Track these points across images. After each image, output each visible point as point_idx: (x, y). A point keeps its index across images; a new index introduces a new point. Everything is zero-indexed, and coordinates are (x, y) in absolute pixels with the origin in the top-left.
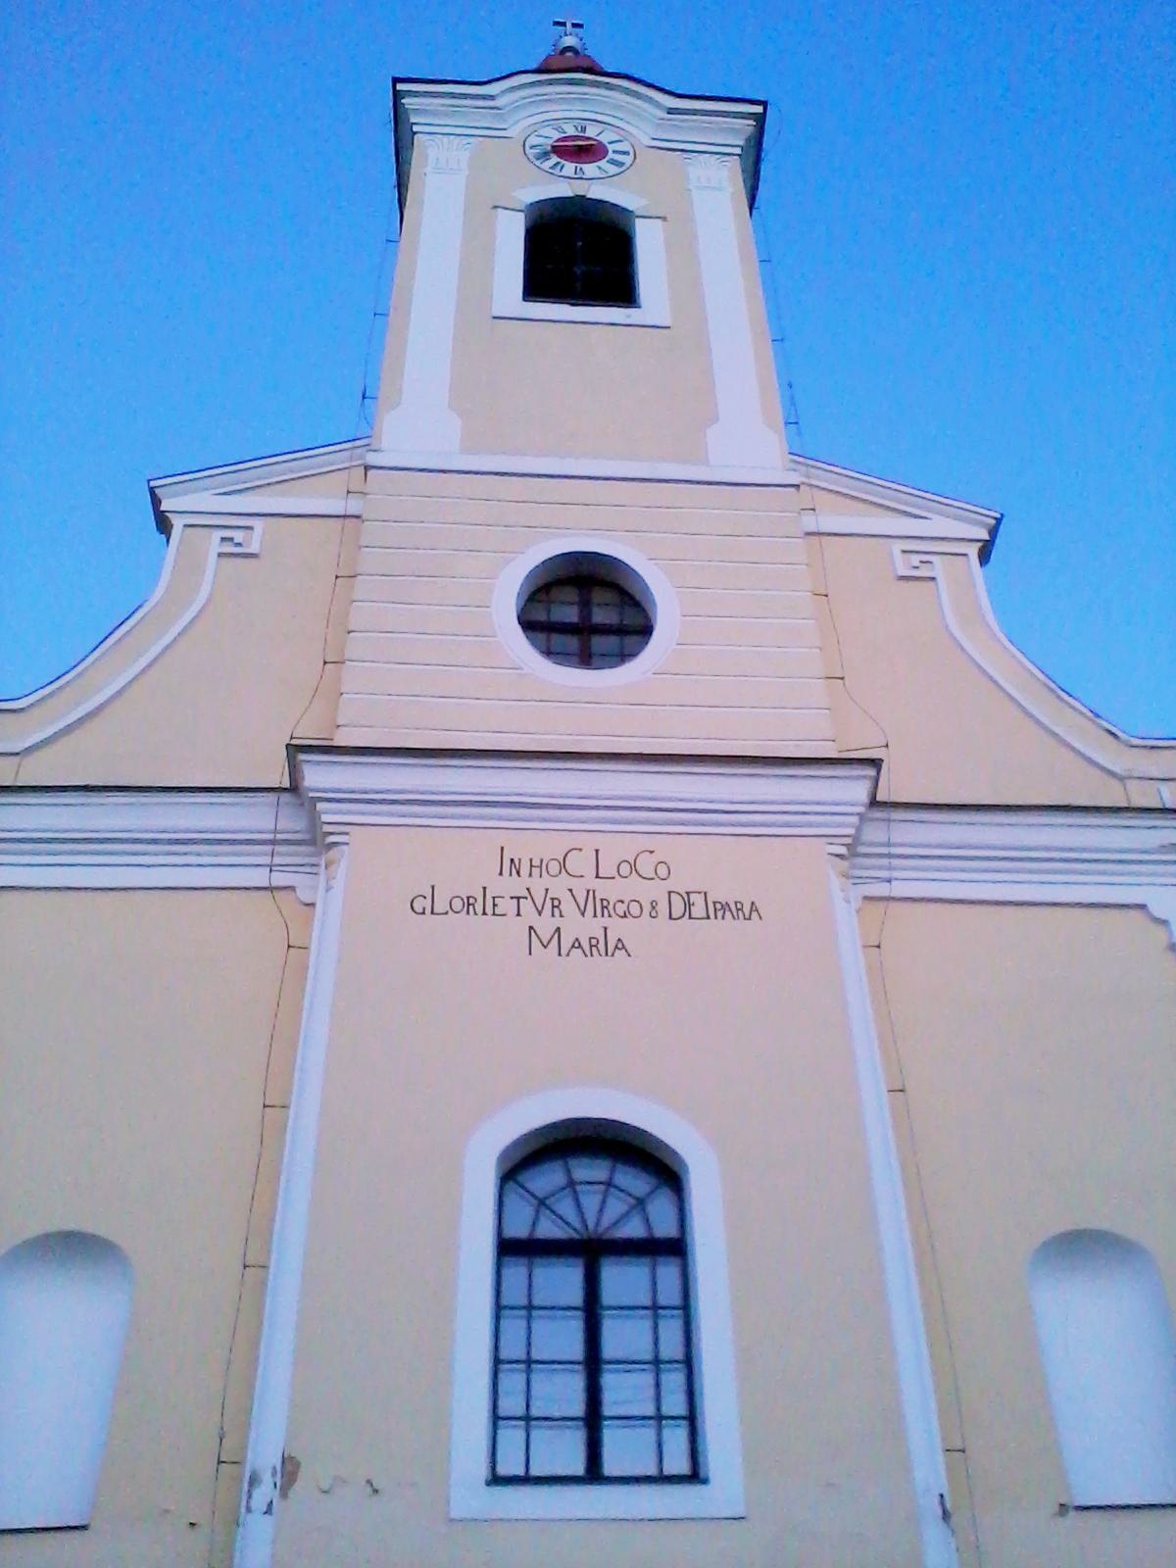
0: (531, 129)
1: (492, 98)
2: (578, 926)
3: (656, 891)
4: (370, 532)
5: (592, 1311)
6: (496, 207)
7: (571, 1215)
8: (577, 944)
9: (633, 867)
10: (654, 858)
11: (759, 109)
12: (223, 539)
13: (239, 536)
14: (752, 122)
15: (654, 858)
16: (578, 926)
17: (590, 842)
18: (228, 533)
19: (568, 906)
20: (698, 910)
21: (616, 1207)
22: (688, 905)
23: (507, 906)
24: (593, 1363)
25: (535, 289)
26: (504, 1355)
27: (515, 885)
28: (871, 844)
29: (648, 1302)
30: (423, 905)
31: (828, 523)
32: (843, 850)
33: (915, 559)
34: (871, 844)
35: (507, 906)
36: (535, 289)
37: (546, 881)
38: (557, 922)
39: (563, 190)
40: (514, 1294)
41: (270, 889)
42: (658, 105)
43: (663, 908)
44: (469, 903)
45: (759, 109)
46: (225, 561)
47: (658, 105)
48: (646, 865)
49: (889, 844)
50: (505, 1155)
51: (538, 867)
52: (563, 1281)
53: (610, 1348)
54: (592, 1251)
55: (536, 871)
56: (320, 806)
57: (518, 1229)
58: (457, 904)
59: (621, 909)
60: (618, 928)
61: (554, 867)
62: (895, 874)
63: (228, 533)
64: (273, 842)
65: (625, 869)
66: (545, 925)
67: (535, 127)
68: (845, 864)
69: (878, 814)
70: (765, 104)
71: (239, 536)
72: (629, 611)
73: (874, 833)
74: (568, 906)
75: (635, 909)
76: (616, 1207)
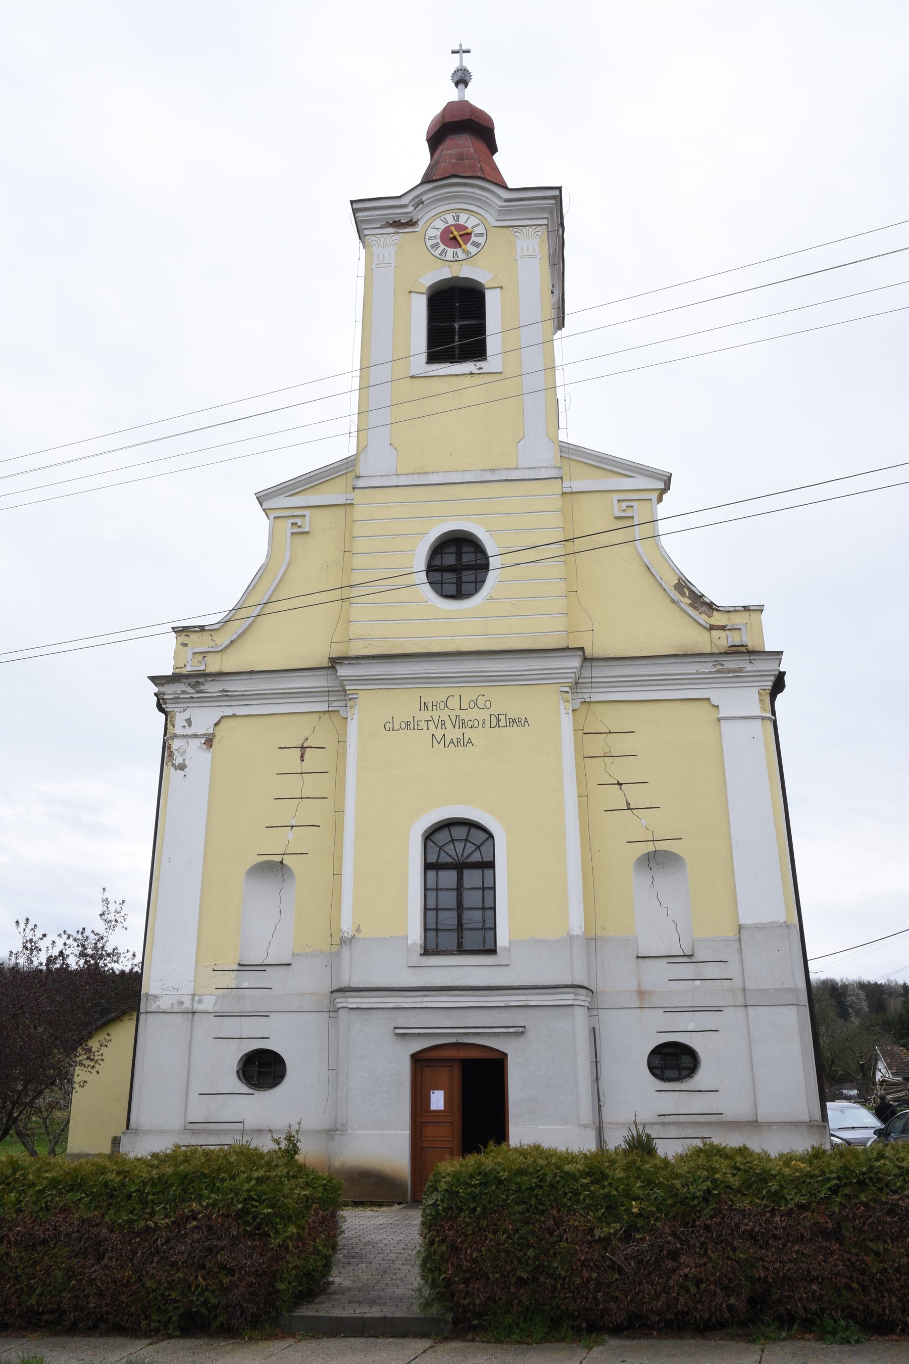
0: (428, 224)
1: (405, 206)
2: (453, 733)
3: (484, 715)
4: (359, 513)
5: (459, 888)
6: (410, 292)
7: (453, 853)
8: (452, 742)
9: (476, 704)
10: (485, 698)
11: (557, 193)
12: (292, 524)
13: (299, 521)
14: (553, 201)
15: (485, 698)
16: (453, 733)
17: (457, 693)
18: (294, 521)
19: (448, 724)
20: (502, 723)
21: (470, 848)
22: (498, 720)
23: (423, 725)
24: (460, 907)
25: (433, 358)
26: (428, 887)
27: (426, 715)
28: (585, 678)
29: (481, 892)
30: (388, 726)
31: (577, 486)
32: (567, 689)
33: (624, 505)
34: (585, 678)
35: (423, 725)
36: (433, 358)
37: (439, 712)
38: (444, 731)
39: (446, 273)
40: (431, 884)
41: (329, 711)
42: (499, 197)
43: (487, 723)
44: (408, 724)
45: (557, 193)
46: (296, 538)
47: (499, 197)
48: (481, 704)
49: (591, 678)
50: (423, 834)
51: (436, 705)
52: (448, 878)
53: (466, 904)
54: (460, 867)
55: (435, 708)
56: (345, 683)
57: (432, 859)
58: (403, 725)
59: (470, 724)
60: (469, 733)
61: (442, 705)
62: (593, 690)
63: (294, 521)
64: (328, 691)
65: (472, 704)
66: (439, 734)
67: (428, 224)
68: (569, 696)
69: (588, 664)
70: (560, 189)
71: (299, 521)
72: (479, 556)
73: (586, 673)
74: (448, 724)
75: (476, 724)
76: (470, 848)
